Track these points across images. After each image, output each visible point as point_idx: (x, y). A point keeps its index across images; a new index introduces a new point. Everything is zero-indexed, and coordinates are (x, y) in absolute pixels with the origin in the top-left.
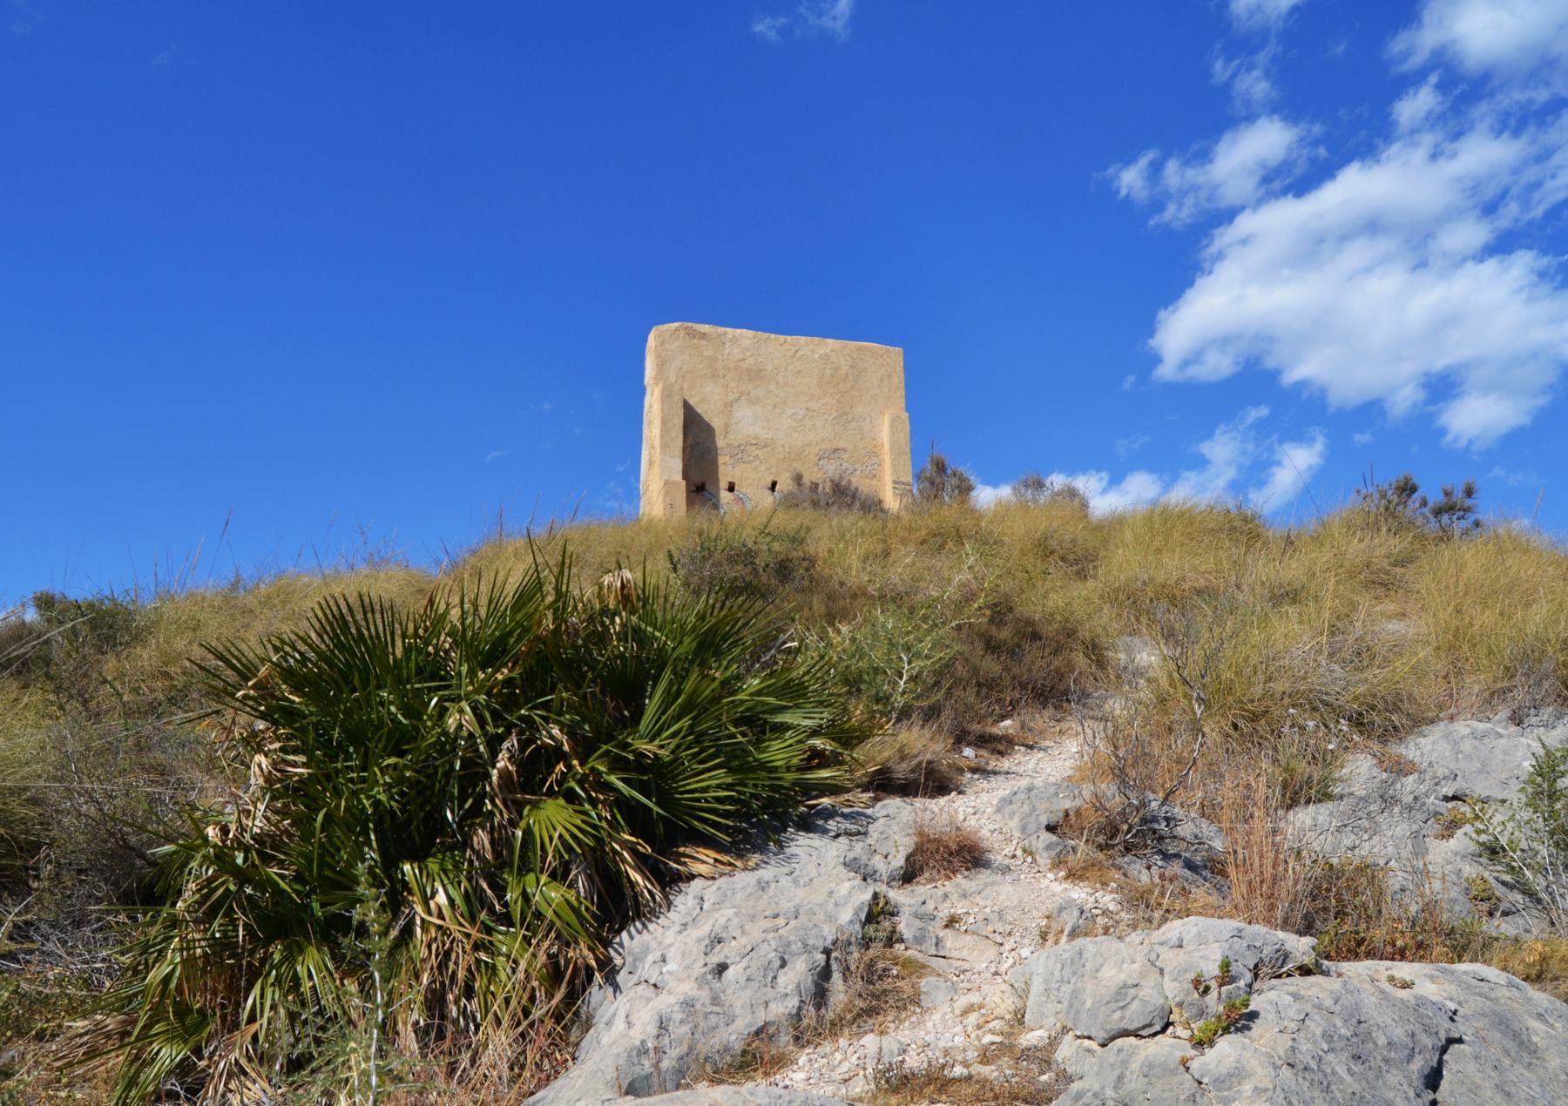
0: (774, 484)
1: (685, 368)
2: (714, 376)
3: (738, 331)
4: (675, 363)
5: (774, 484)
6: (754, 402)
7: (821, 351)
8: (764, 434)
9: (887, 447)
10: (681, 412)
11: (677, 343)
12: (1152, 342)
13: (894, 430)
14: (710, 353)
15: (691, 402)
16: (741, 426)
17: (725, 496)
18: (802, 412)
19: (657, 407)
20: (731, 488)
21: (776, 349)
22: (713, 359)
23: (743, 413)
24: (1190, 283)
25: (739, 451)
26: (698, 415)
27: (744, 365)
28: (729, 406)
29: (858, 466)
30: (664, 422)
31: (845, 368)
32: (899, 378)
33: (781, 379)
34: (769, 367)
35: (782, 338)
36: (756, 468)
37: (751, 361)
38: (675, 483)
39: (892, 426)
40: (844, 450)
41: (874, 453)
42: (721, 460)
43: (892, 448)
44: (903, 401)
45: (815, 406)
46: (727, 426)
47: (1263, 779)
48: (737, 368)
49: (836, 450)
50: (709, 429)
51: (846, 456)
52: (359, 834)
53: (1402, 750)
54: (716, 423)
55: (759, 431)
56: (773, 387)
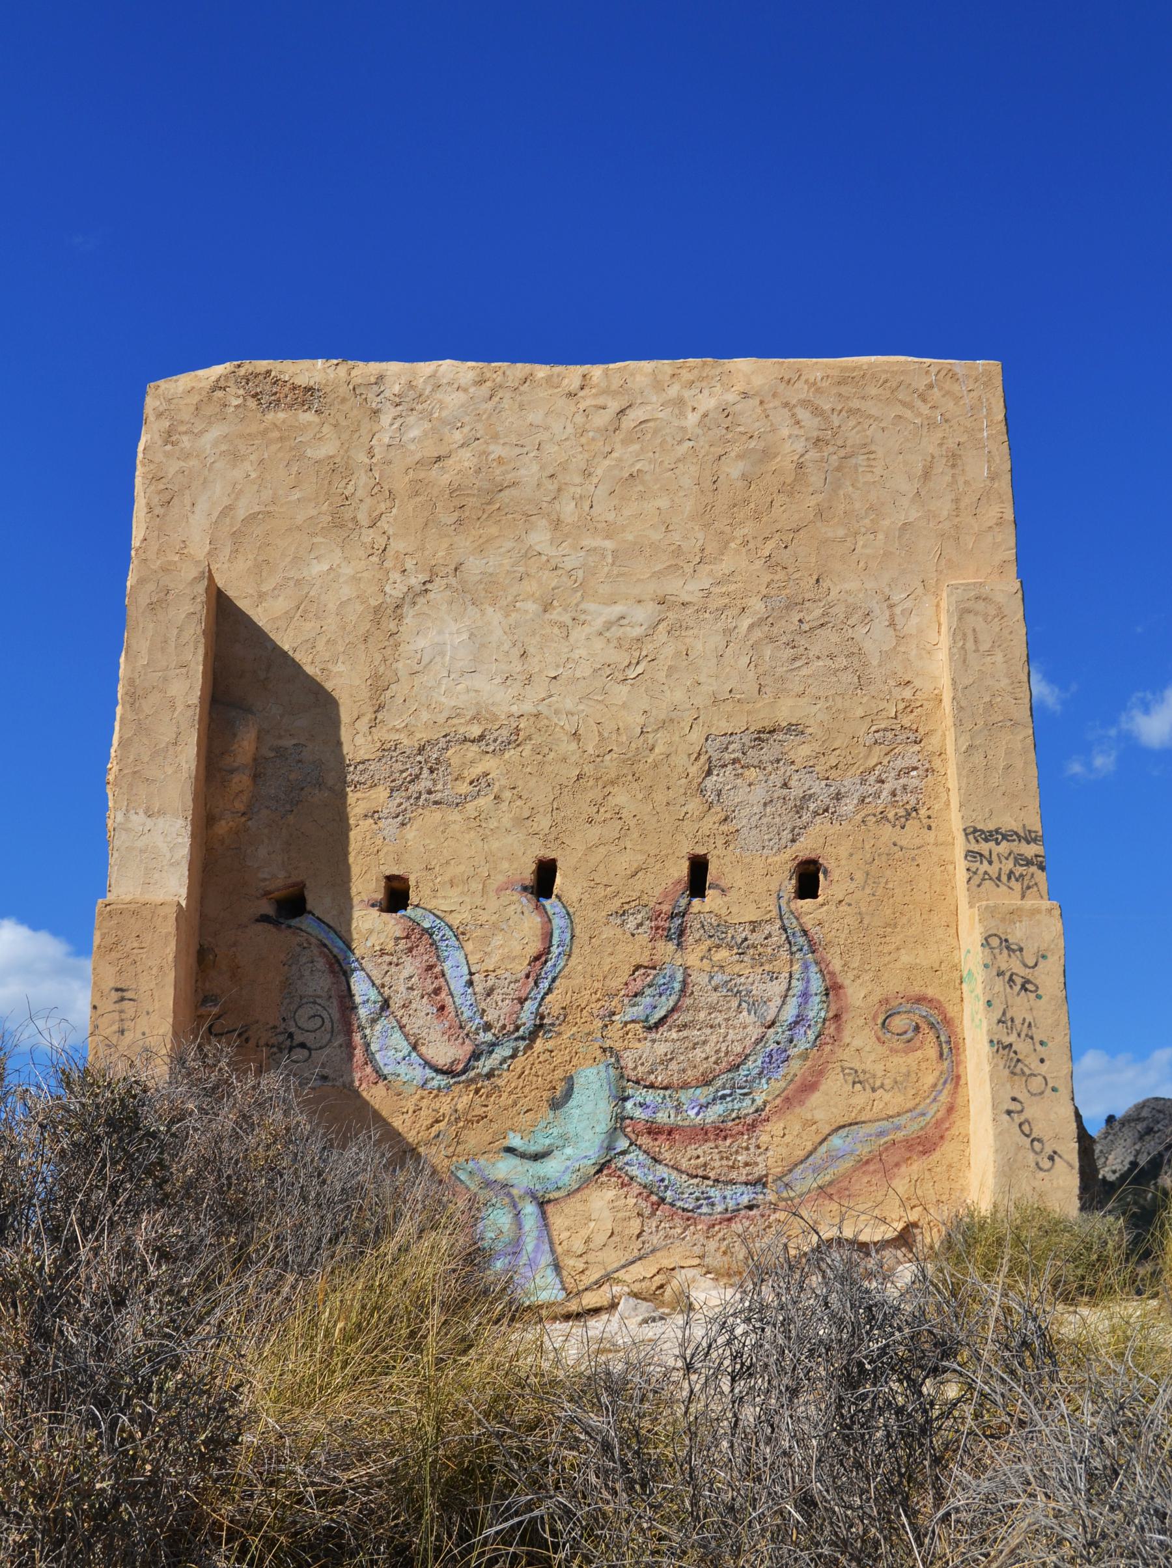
3: (426, 368)
4: (289, 487)
6: (472, 594)
7: (708, 402)
14: (328, 449)
16: (427, 672)
17: (371, 928)
18: (642, 614)
20: (396, 896)
21: (550, 411)
22: (338, 469)
23: (439, 637)
25: (422, 772)
27: (442, 477)
28: (387, 617)
29: (849, 783)
31: (791, 444)
32: (989, 462)
33: (568, 510)
34: (530, 472)
35: (572, 374)
36: (479, 818)
39: (958, 634)
41: (904, 732)
42: (357, 803)
44: (1008, 538)
45: (689, 589)
46: (379, 687)
49: (764, 735)
51: (802, 752)
53: (158, 1073)
54: (345, 681)
56: (540, 538)
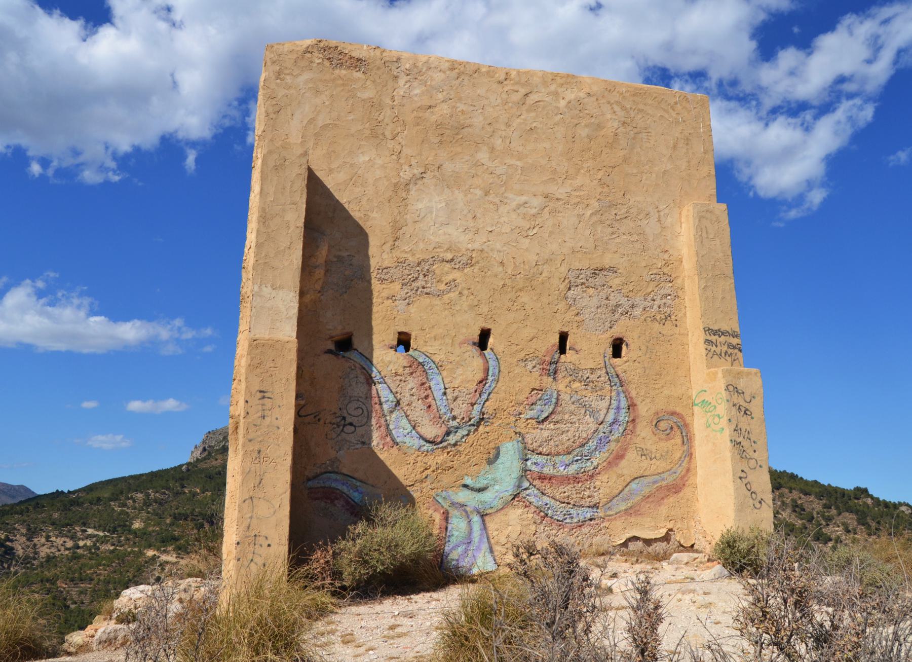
0: (485, 335)
2: (376, 135)
5: (485, 335)
8: (464, 241)
9: (688, 266)
13: (701, 233)
14: (368, 94)
15: (330, 182)
18: (537, 202)
20: (404, 341)
22: (374, 105)
23: (429, 203)
25: (418, 276)
26: (338, 207)
28: (401, 190)
29: (638, 300)
33: (498, 142)
34: (478, 120)
37: (444, 109)
38: (274, 345)
40: (612, 270)
41: (665, 275)
43: (700, 268)
45: (561, 192)
46: (397, 228)
48: (418, 122)
49: (597, 271)
50: (360, 236)
51: (616, 282)
52: (119, 526)
55: (457, 235)
56: (483, 156)
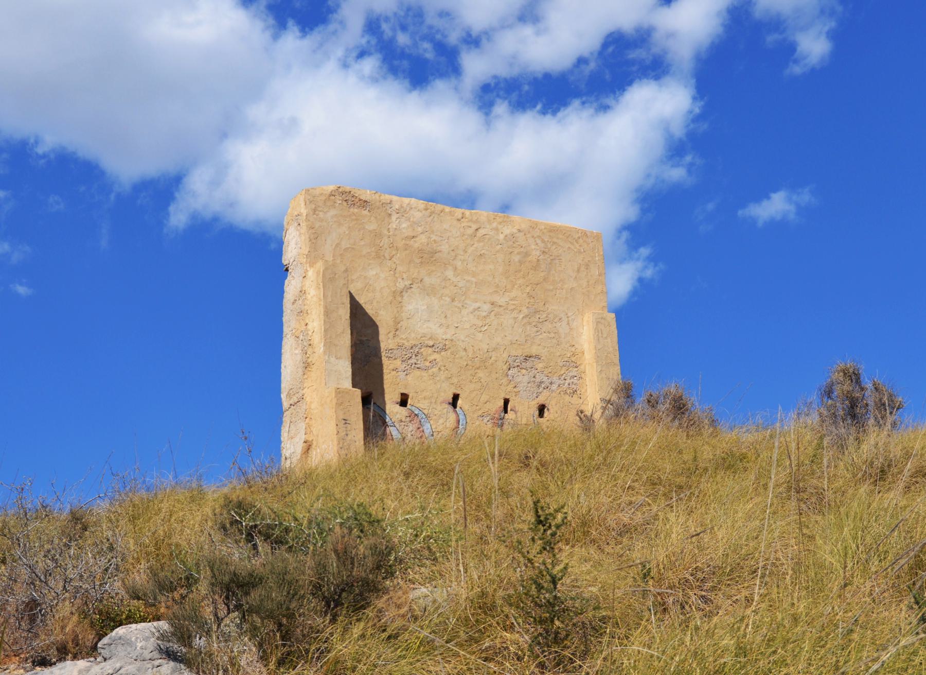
0: (456, 397)
1: (345, 244)
2: (379, 256)
5: (456, 397)
6: (430, 291)
7: (507, 230)
8: (441, 334)
10: (347, 301)
11: (333, 212)
12: (760, 223)
13: (599, 335)
14: (372, 226)
18: (486, 307)
19: (313, 293)
20: (404, 402)
22: (377, 235)
23: (415, 304)
24: (547, 76)
25: (412, 355)
27: (416, 244)
28: (398, 295)
29: (555, 379)
30: (327, 313)
31: (535, 253)
34: (445, 248)
36: (433, 376)
37: (423, 239)
38: (347, 392)
40: (538, 357)
41: (573, 363)
43: (598, 358)
45: (502, 300)
46: (397, 322)
47: (495, 624)
48: (406, 247)
49: (527, 358)
51: (540, 366)
56: (450, 273)
